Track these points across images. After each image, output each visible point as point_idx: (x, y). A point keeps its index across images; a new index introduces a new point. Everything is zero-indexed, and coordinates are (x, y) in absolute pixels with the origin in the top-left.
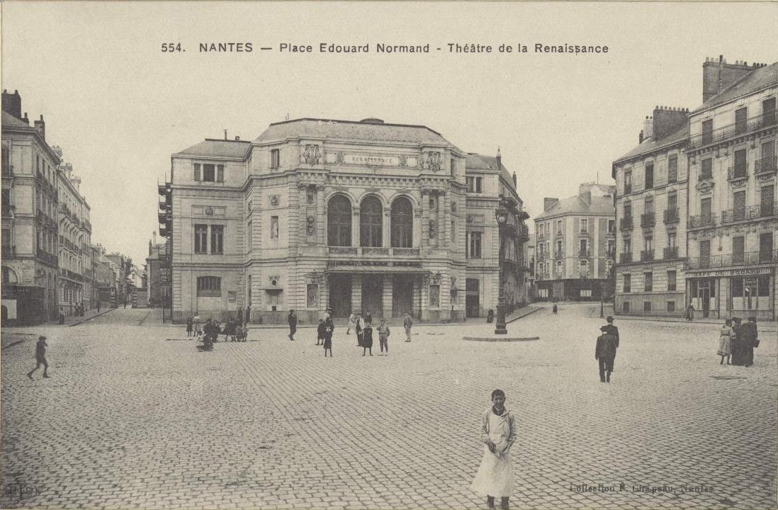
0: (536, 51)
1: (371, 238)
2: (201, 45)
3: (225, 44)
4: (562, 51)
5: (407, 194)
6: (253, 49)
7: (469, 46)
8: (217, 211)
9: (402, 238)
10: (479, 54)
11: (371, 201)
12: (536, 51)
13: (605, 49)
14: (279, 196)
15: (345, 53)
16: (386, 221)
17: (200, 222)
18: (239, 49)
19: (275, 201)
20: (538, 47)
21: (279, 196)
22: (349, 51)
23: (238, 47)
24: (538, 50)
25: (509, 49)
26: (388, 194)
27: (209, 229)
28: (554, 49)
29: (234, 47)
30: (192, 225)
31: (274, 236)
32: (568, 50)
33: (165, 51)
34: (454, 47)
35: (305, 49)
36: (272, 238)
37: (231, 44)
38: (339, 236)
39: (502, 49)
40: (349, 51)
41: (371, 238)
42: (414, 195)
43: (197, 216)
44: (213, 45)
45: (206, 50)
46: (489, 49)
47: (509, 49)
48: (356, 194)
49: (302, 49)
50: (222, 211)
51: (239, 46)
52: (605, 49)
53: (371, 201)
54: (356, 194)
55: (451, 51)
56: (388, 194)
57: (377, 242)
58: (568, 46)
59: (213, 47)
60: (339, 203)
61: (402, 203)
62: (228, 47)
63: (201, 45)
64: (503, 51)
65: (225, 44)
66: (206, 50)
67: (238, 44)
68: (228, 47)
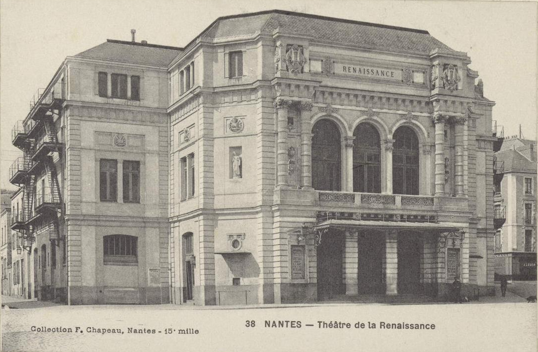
0: (381, 328)
1: (368, 178)
2: (266, 322)
3: (283, 322)
4: (401, 328)
5: (335, 115)
6: (255, 327)
7: (333, 323)
8: (131, 142)
9: (407, 181)
10: (324, 329)
11: (367, 133)
12: (381, 328)
13: (433, 327)
14: (243, 117)
15: (141, 329)
16: (36, 153)
17: (109, 156)
18: (293, 326)
19: (236, 126)
20: (382, 324)
21: (243, 117)
22: (393, 324)
23: (292, 324)
24: (383, 327)
25: (363, 326)
26: (389, 121)
27: (120, 166)
28: (394, 326)
29: (289, 324)
30: (96, 160)
31: (238, 172)
32: (405, 327)
33: (427, 325)
34: (322, 324)
35: (430, 327)
36: (231, 177)
37: (287, 322)
38: (326, 177)
39: (357, 326)
40: (393, 324)
41: (368, 178)
42: (422, 126)
43: (105, 148)
44: (274, 322)
45: (269, 326)
46: (348, 326)
47: (363, 326)
48: (349, 117)
49: (428, 327)
50: (138, 142)
51: (293, 323)
52: (433, 327)
53: (367, 133)
54: (349, 117)
55: (320, 327)
56: (389, 121)
57: (375, 185)
58: (405, 324)
59: (274, 324)
60: (327, 133)
61: (406, 137)
62: (285, 324)
63: (266, 322)
64: (69, 329)
65: (283, 322)
66: (269, 326)
67: (292, 322)
68: (285, 324)
